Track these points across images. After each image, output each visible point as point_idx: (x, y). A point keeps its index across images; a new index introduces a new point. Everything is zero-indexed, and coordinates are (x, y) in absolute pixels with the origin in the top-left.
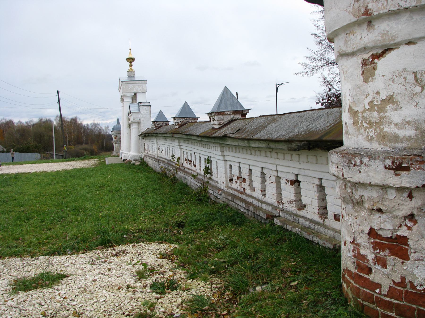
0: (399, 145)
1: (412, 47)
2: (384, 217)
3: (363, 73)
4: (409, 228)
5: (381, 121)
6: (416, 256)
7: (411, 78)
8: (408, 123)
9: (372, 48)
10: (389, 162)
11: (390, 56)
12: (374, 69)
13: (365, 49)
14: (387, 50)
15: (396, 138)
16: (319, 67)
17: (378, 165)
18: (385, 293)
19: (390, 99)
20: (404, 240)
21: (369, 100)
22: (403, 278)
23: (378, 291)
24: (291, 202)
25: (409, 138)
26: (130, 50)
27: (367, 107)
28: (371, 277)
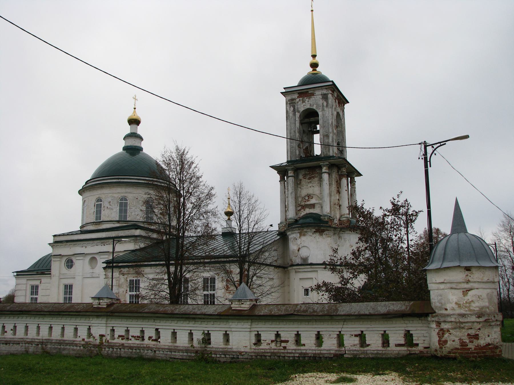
0: (475, 312)
1: (477, 290)
2: (472, 330)
3: (463, 294)
4: (479, 332)
5: (470, 306)
6: (481, 338)
7: (477, 297)
8: (477, 307)
9: (467, 289)
10: (477, 316)
11: (473, 291)
12: (467, 294)
13: (465, 288)
14: (472, 289)
15: (474, 310)
16: (504, 247)
17: (474, 317)
18: (473, 350)
19: (472, 301)
20: (477, 335)
21: (465, 301)
22: (478, 344)
23: (471, 350)
24: (69, 289)
25: (477, 310)
26: (135, 109)
27: (465, 303)
28: (468, 347)
